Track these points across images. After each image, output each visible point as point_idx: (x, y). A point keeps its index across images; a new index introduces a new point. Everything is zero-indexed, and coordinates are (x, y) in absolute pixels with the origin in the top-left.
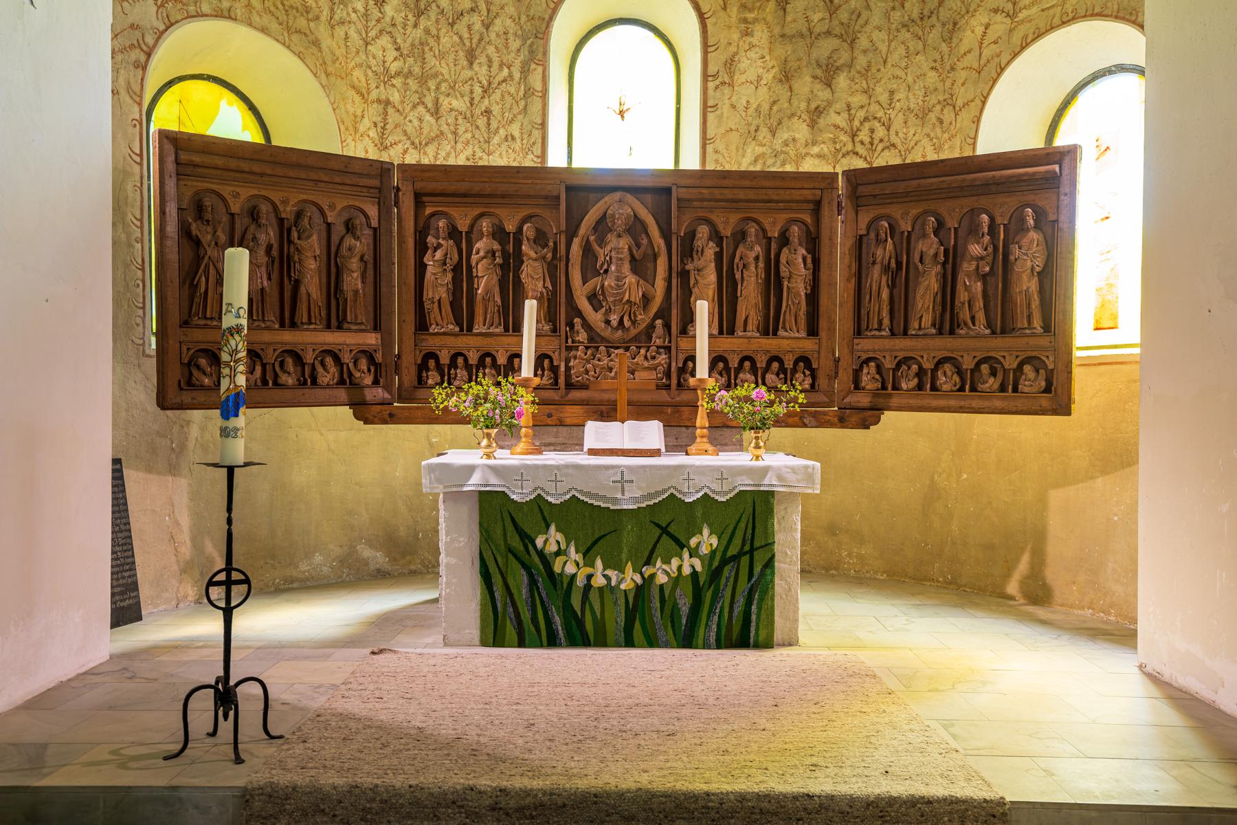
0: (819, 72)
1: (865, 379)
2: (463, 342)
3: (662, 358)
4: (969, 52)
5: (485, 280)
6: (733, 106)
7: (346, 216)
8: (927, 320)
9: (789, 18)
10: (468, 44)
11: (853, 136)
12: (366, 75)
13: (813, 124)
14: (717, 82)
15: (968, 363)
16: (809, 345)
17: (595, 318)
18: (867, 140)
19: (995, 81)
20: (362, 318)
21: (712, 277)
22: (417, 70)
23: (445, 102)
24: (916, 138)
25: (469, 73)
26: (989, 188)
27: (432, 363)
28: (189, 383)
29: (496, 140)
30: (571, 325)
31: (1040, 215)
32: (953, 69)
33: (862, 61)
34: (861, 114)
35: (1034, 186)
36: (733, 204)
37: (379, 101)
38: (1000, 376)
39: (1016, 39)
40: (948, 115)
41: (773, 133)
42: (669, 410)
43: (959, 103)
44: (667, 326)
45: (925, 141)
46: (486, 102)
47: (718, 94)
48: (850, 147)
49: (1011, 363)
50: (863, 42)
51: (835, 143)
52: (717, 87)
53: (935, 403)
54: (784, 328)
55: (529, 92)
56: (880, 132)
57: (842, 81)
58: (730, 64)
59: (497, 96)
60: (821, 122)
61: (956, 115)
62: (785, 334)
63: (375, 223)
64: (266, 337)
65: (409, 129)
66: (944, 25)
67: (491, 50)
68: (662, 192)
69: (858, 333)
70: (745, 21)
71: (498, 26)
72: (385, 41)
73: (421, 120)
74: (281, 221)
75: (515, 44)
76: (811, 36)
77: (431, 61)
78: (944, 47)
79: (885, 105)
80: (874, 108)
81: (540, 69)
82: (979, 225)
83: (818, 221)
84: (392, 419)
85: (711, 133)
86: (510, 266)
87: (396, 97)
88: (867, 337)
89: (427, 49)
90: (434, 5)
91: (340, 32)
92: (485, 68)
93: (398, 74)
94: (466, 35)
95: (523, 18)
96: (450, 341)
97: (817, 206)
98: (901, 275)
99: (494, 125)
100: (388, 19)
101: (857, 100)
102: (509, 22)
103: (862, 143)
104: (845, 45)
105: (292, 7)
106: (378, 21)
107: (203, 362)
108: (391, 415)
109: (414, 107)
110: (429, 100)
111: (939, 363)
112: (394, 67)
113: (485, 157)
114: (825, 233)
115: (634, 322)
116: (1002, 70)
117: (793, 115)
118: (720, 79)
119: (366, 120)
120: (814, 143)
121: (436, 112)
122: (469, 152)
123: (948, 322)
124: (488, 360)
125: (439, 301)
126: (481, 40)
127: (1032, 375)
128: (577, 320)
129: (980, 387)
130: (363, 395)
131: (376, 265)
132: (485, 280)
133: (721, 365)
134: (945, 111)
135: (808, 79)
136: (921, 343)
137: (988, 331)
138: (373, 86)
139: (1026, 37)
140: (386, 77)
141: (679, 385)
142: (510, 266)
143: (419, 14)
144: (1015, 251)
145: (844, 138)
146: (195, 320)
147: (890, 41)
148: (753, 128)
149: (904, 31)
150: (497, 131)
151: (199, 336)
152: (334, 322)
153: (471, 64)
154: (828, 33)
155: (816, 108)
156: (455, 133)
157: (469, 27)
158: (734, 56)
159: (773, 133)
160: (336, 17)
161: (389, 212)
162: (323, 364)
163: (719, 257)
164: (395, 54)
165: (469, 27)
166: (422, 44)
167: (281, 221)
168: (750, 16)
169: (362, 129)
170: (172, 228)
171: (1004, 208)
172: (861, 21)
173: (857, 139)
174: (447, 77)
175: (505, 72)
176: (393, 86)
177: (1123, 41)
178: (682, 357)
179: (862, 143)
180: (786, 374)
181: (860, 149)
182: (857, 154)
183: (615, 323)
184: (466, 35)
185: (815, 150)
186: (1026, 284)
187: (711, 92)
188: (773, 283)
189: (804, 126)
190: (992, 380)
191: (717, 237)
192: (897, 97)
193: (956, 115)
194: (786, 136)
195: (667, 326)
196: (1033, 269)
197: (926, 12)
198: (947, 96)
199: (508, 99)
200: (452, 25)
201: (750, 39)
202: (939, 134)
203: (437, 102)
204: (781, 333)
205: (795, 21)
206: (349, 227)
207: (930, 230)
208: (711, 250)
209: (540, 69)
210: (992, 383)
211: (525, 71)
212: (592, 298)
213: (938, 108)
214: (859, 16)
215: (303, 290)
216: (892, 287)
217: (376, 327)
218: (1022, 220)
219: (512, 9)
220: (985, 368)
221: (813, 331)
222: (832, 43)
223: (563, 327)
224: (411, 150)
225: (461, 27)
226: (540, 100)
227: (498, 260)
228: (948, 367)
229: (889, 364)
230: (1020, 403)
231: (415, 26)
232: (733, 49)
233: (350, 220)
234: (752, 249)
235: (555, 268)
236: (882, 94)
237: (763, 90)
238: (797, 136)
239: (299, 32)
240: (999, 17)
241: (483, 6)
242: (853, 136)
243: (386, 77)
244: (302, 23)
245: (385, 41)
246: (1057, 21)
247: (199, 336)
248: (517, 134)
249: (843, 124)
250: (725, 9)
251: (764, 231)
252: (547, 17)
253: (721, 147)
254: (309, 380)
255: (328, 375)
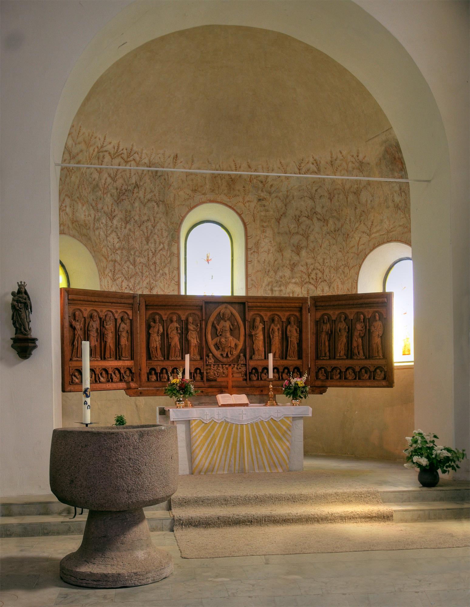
0: (294, 248)
1: (320, 376)
2: (166, 364)
3: (243, 369)
4: (354, 246)
5: (176, 340)
6: (259, 261)
7: (121, 315)
8: (342, 353)
9: (281, 226)
10: (146, 234)
11: (309, 276)
12: (107, 250)
13: (292, 270)
14: (252, 251)
15: (357, 369)
16: (298, 363)
17: (217, 353)
18: (315, 278)
19: (364, 260)
20: (127, 355)
21: (261, 337)
22: (126, 246)
23: (138, 260)
24: (335, 278)
25: (147, 247)
26: (362, 305)
27: (153, 372)
28: (72, 382)
29: (159, 275)
30: (208, 356)
31: (381, 315)
32: (348, 252)
33: (311, 246)
34: (312, 267)
35: (378, 306)
36: (269, 308)
37: (112, 261)
38: (369, 373)
39: (371, 244)
40: (347, 270)
41: (276, 272)
42: (248, 389)
43: (351, 266)
44: (245, 356)
45: (338, 280)
46: (154, 259)
47: (252, 256)
48: (307, 280)
49: (372, 369)
50: (312, 238)
51: (301, 278)
52: (252, 253)
53: (346, 384)
54: (289, 355)
55: (172, 254)
56: (320, 275)
57: (303, 253)
58: (257, 244)
59: (158, 256)
60: (296, 269)
61: (350, 270)
62: (290, 359)
63: (131, 318)
64: (96, 363)
65: (124, 272)
66: (344, 234)
67: (156, 237)
68: (241, 304)
69: (317, 358)
70: (263, 226)
71: (158, 227)
72: (114, 235)
73: (128, 268)
74: (100, 319)
75: (165, 234)
76: (290, 234)
77: (132, 243)
78: (344, 243)
79: (321, 264)
80: (317, 265)
81: (176, 245)
82: (360, 319)
83: (301, 315)
84: (141, 394)
85: (249, 272)
86: (184, 333)
87: (118, 258)
88: (320, 359)
89: (130, 237)
90: (132, 219)
91: (97, 232)
92: (153, 245)
93: (119, 249)
94: (145, 231)
95: (169, 223)
96: (160, 363)
97: (300, 309)
98: (332, 335)
99: (158, 269)
100: (115, 226)
101: (310, 261)
102: (163, 225)
103: (313, 279)
104: (304, 239)
105: (81, 225)
106: (111, 227)
107: (77, 374)
108: (141, 393)
109: (126, 262)
110: (131, 259)
111: (347, 369)
112: (117, 246)
113: (154, 282)
114: (304, 320)
115: (232, 355)
116: (367, 255)
117: (283, 266)
118: (253, 250)
119: (108, 269)
120: (293, 278)
121: (134, 264)
122: (148, 280)
123: (350, 354)
124: (164, 371)
125: (156, 347)
126: (151, 233)
127: (379, 373)
128: (211, 354)
129: (362, 378)
130: (130, 385)
131: (131, 333)
132: (176, 340)
133: (275, 370)
134: (345, 268)
135: (289, 251)
136: (340, 362)
137: (364, 357)
138: (109, 254)
139: (374, 244)
140: (114, 250)
141: (250, 379)
142: (184, 333)
143: (127, 222)
144: (373, 329)
145: (305, 276)
146: (74, 359)
147: (323, 239)
148: (267, 271)
149: (328, 235)
150: (159, 272)
151: (74, 364)
152: (118, 357)
153: (148, 243)
154: (297, 233)
155: (294, 263)
156: (142, 273)
157: (147, 228)
158: (259, 240)
159: (276, 272)
160: (96, 227)
161: (136, 313)
162: (114, 373)
163: (264, 329)
164: (117, 240)
165: (147, 228)
166: (128, 235)
167: (100, 319)
168: (265, 224)
169: (106, 273)
170: (67, 324)
171: (368, 312)
172: (310, 229)
173: (310, 277)
174: (138, 249)
175: (162, 246)
176: (117, 254)
177: (405, 251)
178: (250, 368)
179: (313, 279)
180: (258, 374)
181: (311, 281)
182: (311, 283)
183: (225, 355)
184: (145, 231)
185: (293, 281)
186: (377, 340)
187: (249, 256)
188: (285, 338)
189: (289, 270)
190: (366, 375)
191: (263, 321)
192: (326, 261)
193: (350, 270)
194: (281, 274)
195: (245, 356)
196: (379, 335)
197: (337, 229)
198: (346, 263)
199: (163, 257)
200: (140, 227)
201: (265, 234)
202: (343, 277)
203: (134, 260)
204: (288, 358)
205: (283, 227)
206: (122, 319)
207: (342, 319)
208: (261, 326)
209: (176, 245)
210: (366, 376)
211: (170, 245)
212: (217, 346)
213: (342, 267)
214: (310, 227)
215: (108, 345)
216: (329, 340)
217: (132, 359)
218: (375, 316)
219: (164, 219)
220: (363, 370)
221: (300, 357)
222: (299, 237)
223: (205, 357)
224: (125, 281)
225: (143, 227)
226: (176, 258)
227: (179, 331)
228: (350, 371)
229: (329, 369)
230: (376, 383)
231: (125, 228)
232: (258, 238)
233: (123, 317)
234: (276, 326)
235: (202, 334)
236: (320, 258)
237: (270, 255)
238: (286, 274)
239: (84, 235)
240: (365, 235)
241: (152, 219)
242: (309, 276)
243: (114, 250)
244: (85, 231)
245: (114, 235)
246: (385, 240)
247: (74, 364)
248: (167, 272)
249: (305, 271)
250: (254, 221)
251: (280, 318)
252: (179, 223)
253: (254, 278)
254: (110, 380)
255: (116, 378)
